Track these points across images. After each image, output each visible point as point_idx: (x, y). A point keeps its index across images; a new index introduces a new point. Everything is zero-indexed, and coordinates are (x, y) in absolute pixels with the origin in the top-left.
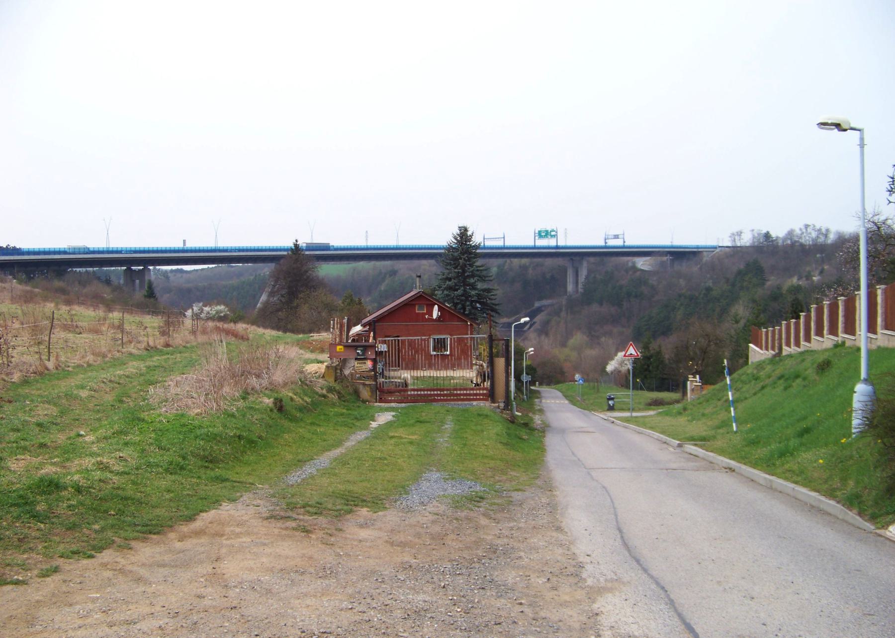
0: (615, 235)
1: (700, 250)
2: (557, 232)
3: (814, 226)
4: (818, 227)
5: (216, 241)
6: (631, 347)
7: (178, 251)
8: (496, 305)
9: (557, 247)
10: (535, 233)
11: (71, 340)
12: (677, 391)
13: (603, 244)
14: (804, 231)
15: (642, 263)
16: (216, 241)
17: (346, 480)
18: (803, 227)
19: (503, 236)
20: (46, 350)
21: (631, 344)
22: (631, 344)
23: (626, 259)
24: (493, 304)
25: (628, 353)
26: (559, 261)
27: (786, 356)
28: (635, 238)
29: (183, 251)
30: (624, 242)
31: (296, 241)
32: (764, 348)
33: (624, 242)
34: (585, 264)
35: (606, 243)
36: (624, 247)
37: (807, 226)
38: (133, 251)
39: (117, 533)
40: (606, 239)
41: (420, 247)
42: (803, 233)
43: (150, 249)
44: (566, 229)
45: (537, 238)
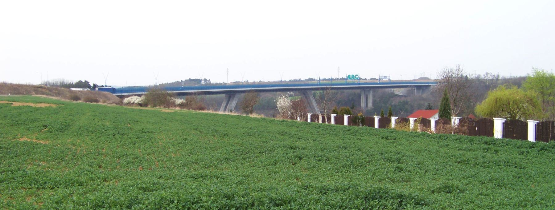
1: (429, 84)
3: (491, 74)
4: (493, 74)
11: (341, 192)
14: (486, 76)
15: (397, 92)
18: (485, 74)
19: (389, 76)
20: (243, 177)
23: (387, 89)
26: (358, 91)
27: (501, 117)
28: (395, 77)
31: (498, 73)
34: (371, 92)
37: (487, 74)
39: (153, 125)
42: (485, 77)
44: (339, 67)
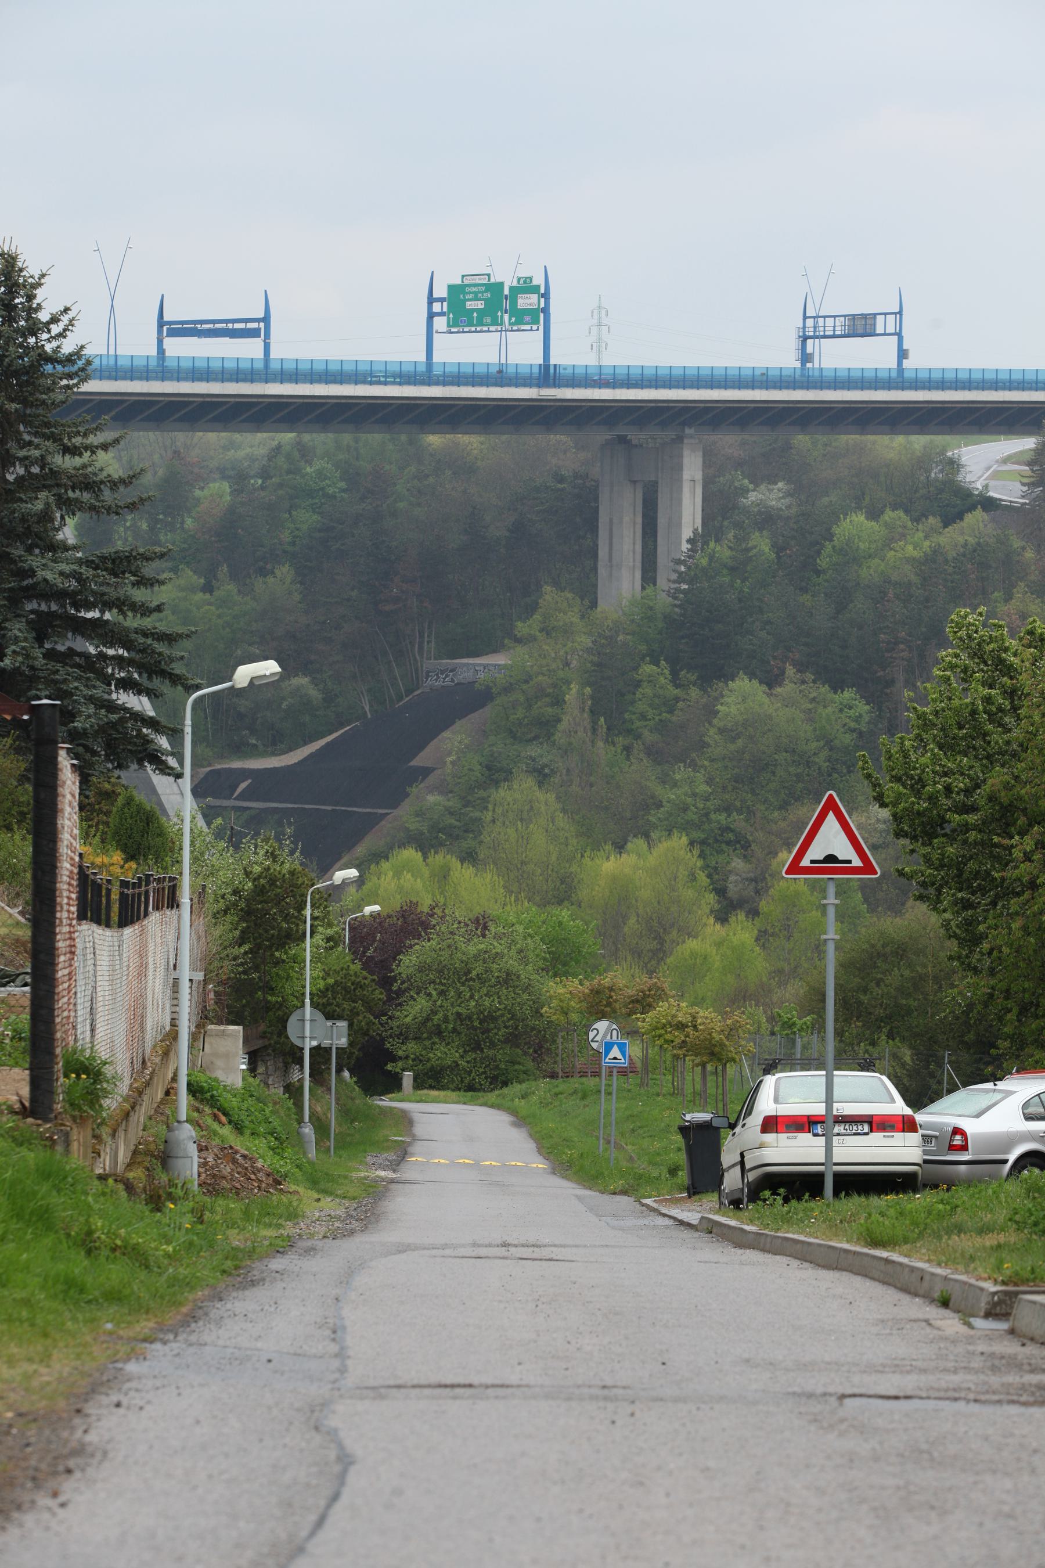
0: (853, 318)
2: (546, 296)
5: (599, 345)
6: (831, 816)
7: (876, 383)
8: (170, 639)
9: (547, 375)
10: (431, 300)
12: (492, 1097)
13: (787, 360)
16: (599, 345)
17: (790, 1390)
21: (831, 805)
22: (831, 805)
24: (145, 634)
25: (816, 852)
29: (428, 378)
30: (903, 354)
32: (103, 921)
33: (903, 354)
35: (806, 358)
36: (899, 381)
38: (334, 375)
40: (804, 339)
41: (334, 367)
43: (347, 368)
45: (440, 323)
